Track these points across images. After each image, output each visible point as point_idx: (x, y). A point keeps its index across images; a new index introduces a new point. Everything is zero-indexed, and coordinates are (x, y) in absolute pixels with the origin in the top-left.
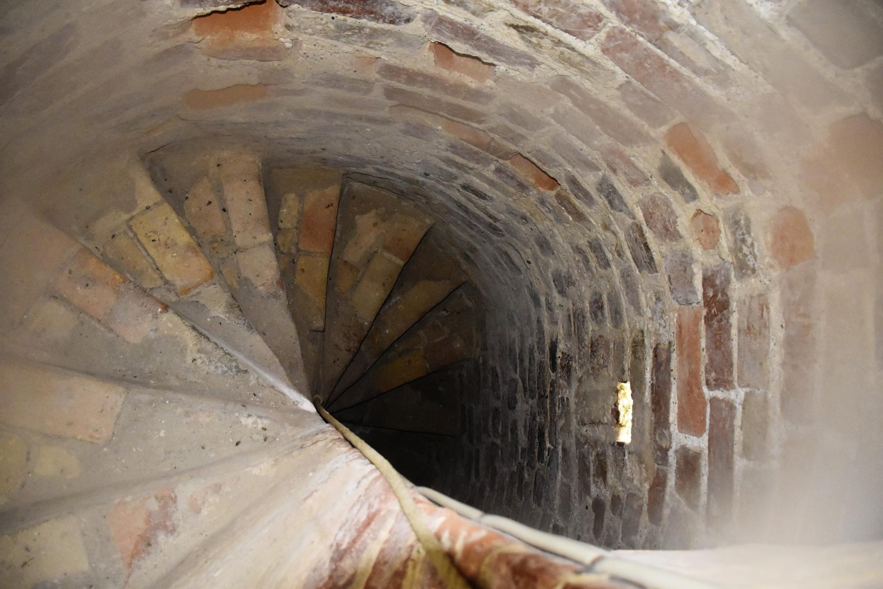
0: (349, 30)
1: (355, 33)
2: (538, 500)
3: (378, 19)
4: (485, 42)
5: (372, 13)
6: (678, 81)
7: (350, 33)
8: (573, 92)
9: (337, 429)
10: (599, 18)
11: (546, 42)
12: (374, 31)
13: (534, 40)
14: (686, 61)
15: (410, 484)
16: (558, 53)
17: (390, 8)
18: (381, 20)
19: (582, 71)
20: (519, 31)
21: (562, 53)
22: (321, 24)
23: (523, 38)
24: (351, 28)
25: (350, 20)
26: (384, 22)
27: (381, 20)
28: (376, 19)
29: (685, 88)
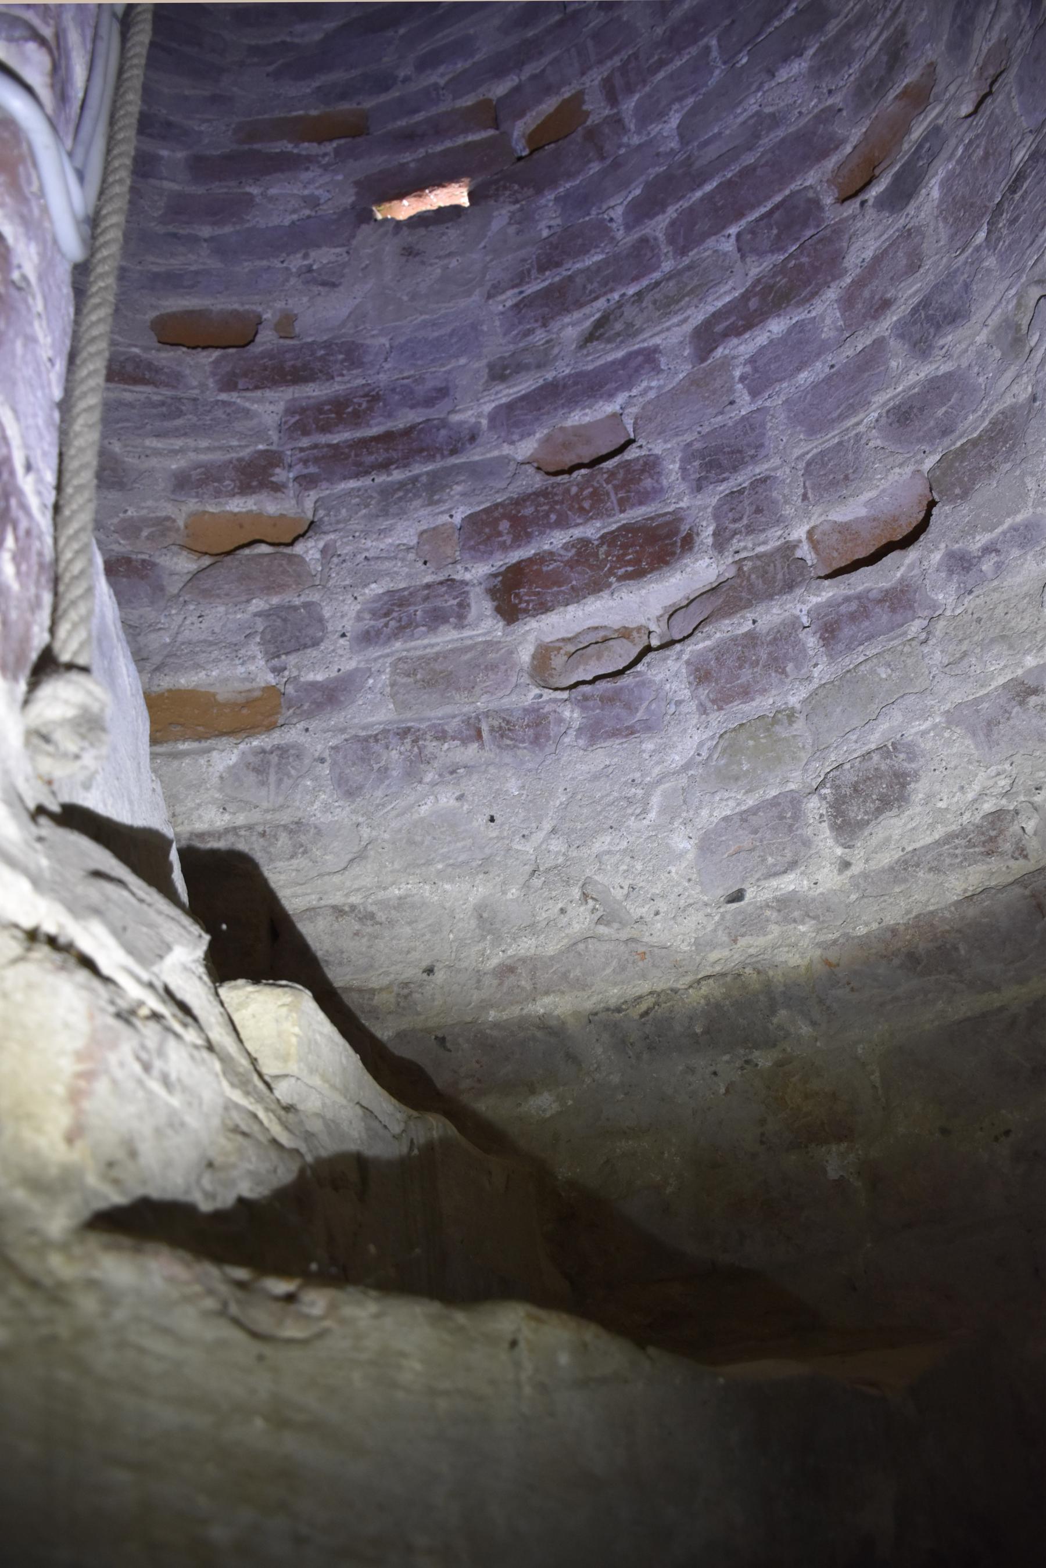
0: (399, 489)
1: (408, 491)
2: (747, 792)
3: (434, 456)
4: (576, 383)
5: (422, 450)
6: (754, 169)
7: (401, 494)
8: (719, 328)
9: (65, 406)
10: (683, 252)
11: (629, 312)
12: (433, 475)
13: (618, 326)
14: (734, 154)
15: (154, 1192)
16: (651, 306)
17: (443, 432)
18: (438, 456)
19: (692, 291)
20: (598, 339)
21: (655, 302)
22: (358, 496)
23: (609, 341)
24: (401, 485)
25: (397, 475)
26: (443, 457)
27: (438, 456)
28: (431, 458)
29: (767, 162)
